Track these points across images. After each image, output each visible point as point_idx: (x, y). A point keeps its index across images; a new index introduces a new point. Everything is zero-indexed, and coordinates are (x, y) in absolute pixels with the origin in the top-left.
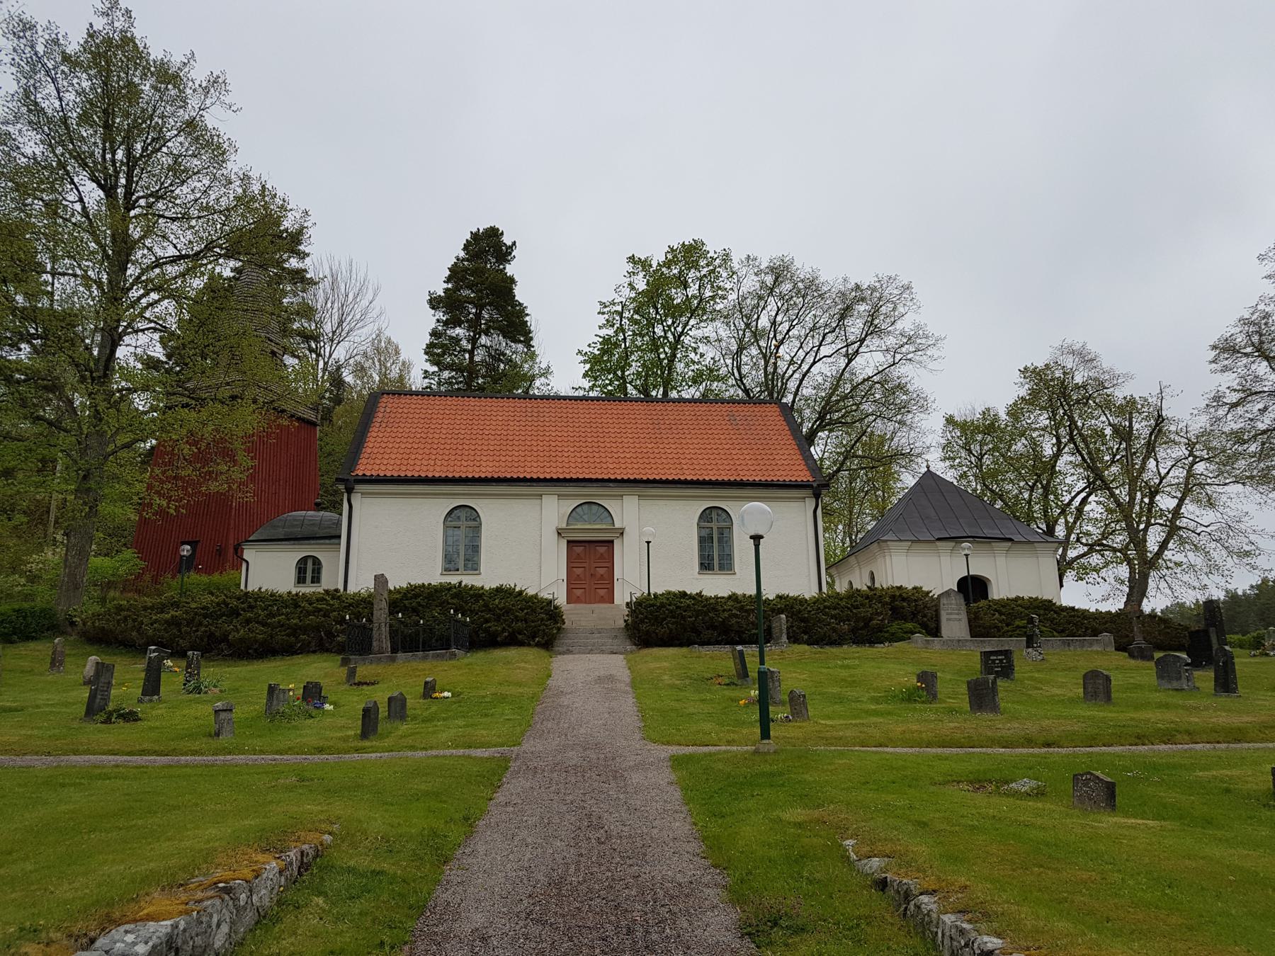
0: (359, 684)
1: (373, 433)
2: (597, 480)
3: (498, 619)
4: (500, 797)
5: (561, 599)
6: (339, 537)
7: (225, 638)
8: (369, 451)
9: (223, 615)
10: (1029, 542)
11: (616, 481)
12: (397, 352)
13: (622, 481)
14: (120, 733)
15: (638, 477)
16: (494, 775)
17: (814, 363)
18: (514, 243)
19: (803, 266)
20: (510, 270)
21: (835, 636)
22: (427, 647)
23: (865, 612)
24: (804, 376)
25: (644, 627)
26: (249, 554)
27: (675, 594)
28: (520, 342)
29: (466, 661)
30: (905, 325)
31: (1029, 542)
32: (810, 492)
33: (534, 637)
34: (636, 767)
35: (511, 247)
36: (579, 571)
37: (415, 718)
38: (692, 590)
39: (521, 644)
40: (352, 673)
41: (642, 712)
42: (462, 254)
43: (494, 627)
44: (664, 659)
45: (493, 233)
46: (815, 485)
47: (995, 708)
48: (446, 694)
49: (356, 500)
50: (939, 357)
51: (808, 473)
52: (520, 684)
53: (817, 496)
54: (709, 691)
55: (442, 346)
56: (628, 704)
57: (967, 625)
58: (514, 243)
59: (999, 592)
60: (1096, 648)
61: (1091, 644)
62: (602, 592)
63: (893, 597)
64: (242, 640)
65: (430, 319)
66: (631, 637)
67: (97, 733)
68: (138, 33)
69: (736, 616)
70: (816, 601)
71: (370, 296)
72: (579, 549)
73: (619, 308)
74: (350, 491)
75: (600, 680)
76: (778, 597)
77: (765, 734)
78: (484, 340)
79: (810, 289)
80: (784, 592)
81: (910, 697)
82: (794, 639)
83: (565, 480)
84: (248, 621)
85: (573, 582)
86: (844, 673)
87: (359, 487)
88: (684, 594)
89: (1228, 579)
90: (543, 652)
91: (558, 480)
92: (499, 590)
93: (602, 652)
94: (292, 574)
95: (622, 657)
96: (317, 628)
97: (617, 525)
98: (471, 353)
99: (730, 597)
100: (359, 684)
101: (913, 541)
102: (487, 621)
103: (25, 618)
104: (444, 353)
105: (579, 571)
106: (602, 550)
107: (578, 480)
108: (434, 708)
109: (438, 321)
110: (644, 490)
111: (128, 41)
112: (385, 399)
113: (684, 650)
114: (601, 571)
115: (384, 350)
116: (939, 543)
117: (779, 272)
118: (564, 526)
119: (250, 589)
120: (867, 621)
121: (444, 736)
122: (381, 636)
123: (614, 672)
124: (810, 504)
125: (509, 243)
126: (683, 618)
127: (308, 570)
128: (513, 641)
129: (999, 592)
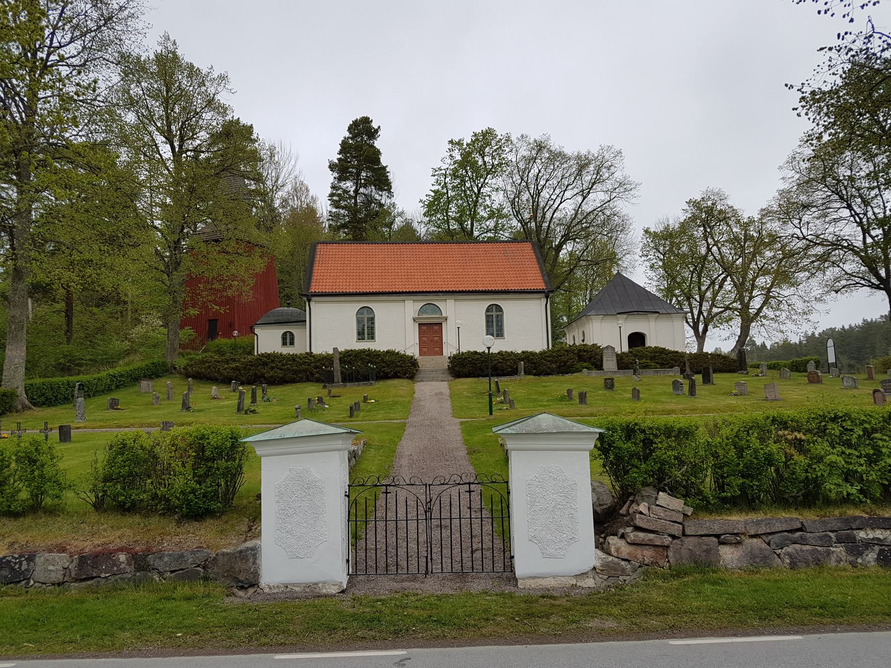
0: (333, 397)
1: (316, 267)
2: (433, 292)
3: (388, 366)
4: (406, 433)
5: (417, 355)
6: (305, 321)
7: (263, 376)
8: (315, 278)
9: (260, 365)
10: (668, 314)
11: (442, 292)
12: (307, 190)
13: (446, 292)
14: (251, 417)
15: (454, 289)
16: (403, 427)
17: (561, 203)
18: (379, 127)
19: (555, 144)
20: (378, 144)
21: (549, 371)
22: (358, 380)
23: (564, 358)
24: (555, 211)
25: (457, 369)
26: (257, 331)
27: (472, 353)
28: (385, 190)
29: (377, 386)
30: (618, 175)
32: (544, 295)
33: (405, 374)
34: (448, 425)
35: (377, 130)
36: (425, 339)
37: (364, 410)
39: (400, 377)
40: (330, 392)
41: (453, 409)
42: (347, 134)
43: (387, 370)
44: (466, 384)
45: (366, 121)
46: (546, 291)
47: (585, 403)
48: (373, 401)
49: (312, 304)
50: (637, 196)
51: (543, 284)
52: (402, 397)
53: (547, 297)
54: (482, 398)
55: (339, 195)
56: (448, 404)
58: (379, 127)
59: (651, 342)
60: (670, 374)
61: (669, 372)
62: (437, 349)
63: (580, 351)
64: (272, 377)
65: (330, 177)
66: (451, 373)
68: (179, 52)
69: (501, 362)
70: (542, 353)
71: (293, 162)
72: (424, 328)
73: (444, 172)
74: (309, 301)
75: (436, 394)
76: (523, 352)
77: (491, 414)
78: (362, 190)
79: (557, 157)
80: (525, 350)
81: (562, 399)
82: (527, 372)
83: (416, 292)
84: (273, 368)
85: (422, 344)
86: (542, 389)
87: (314, 299)
88: (476, 353)
89: (800, 326)
90: (410, 381)
91: (413, 292)
92: (388, 352)
93: (437, 381)
94: (280, 341)
95: (446, 383)
96: (305, 371)
97: (444, 315)
98: (355, 198)
99: (499, 353)
100: (333, 397)
101: (604, 315)
102: (384, 367)
103: (156, 367)
104: (340, 200)
105: (425, 339)
106: (436, 328)
107: (423, 292)
108: (369, 407)
109: (335, 178)
111: (176, 57)
112: (319, 246)
113: (476, 379)
114: (436, 339)
115: (299, 189)
116: (618, 316)
117: (540, 147)
118: (417, 316)
119: (316, 351)
120: (565, 363)
121: (379, 416)
122: (338, 376)
123: (442, 390)
124: (544, 301)
125: (376, 127)
126: (476, 364)
127: (288, 339)
128: (396, 376)
129: (651, 342)
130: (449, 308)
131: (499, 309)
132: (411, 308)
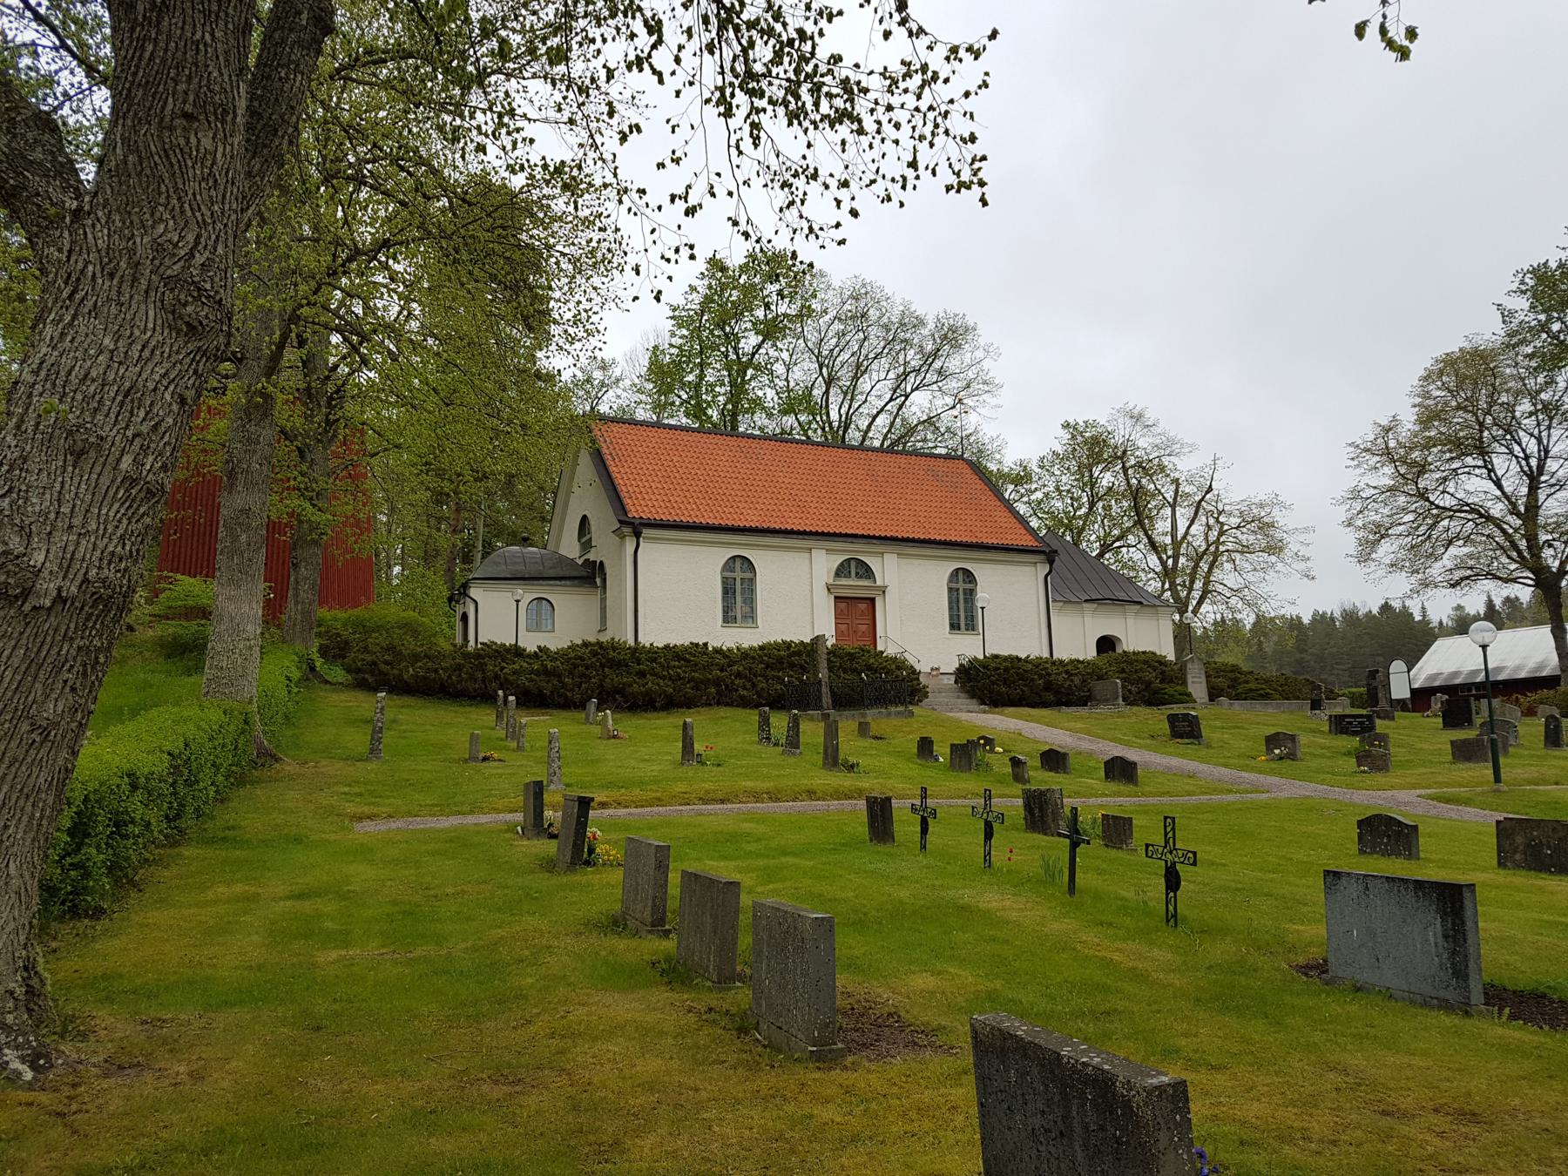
2: (863, 536)
13: (886, 538)
31: (1155, 606)
32: (1042, 557)
38: (714, 643)
57: (407, 700)
67: (691, 770)
83: (835, 535)
87: (646, 532)
97: (879, 583)
106: (863, 606)
110: (795, 541)
116: (1085, 605)
118: (831, 581)
119: (645, 640)
130: (889, 569)
131: (969, 576)
132: (823, 563)
